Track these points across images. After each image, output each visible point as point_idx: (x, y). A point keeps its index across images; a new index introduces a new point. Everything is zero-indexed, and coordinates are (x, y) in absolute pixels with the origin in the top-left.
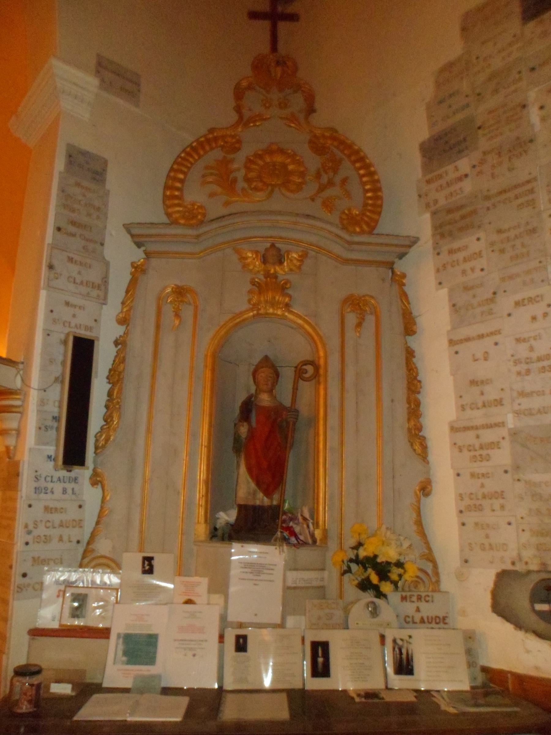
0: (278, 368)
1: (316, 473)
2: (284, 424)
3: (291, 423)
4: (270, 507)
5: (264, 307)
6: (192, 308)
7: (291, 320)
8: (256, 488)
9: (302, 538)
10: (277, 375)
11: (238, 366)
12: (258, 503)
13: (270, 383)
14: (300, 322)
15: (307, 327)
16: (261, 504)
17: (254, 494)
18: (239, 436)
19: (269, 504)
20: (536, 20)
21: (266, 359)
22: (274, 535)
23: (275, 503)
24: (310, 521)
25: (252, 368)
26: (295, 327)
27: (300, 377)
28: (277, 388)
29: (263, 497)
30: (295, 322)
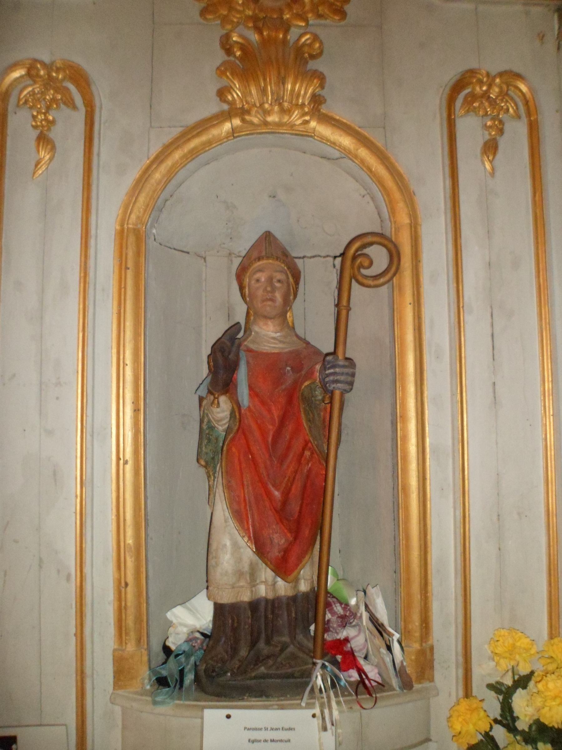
0: (297, 261)
1: (167, 182)
2: (319, 394)
3: (337, 393)
4: (294, 599)
5: (258, 105)
6: (80, 116)
7: (324, 140)
8: (256, 558)
9: (372, 672)
10: (296, 276)
11: (205, 259)
12: (262, 591)
13: (279, 296)
14: (346, 141)
15: (363, 153)
16: (271, 596)
17: (253, 572)
18: (212, 428)
19: (290, 593)
20: (291, 252)
21: (268, 237)
22: (307, 684)
23: (304, 587)
24: (393, 635)
25: (237, 262)
26: (337, 154)
27: (353, 277)
28: (297, 305)
29: (274, 579)
30: (333, 144)
